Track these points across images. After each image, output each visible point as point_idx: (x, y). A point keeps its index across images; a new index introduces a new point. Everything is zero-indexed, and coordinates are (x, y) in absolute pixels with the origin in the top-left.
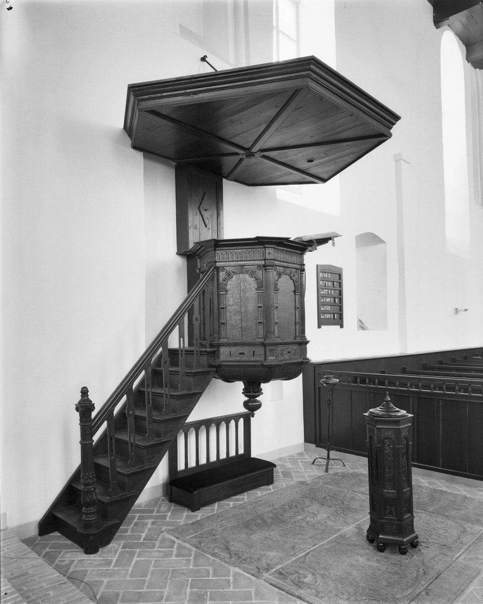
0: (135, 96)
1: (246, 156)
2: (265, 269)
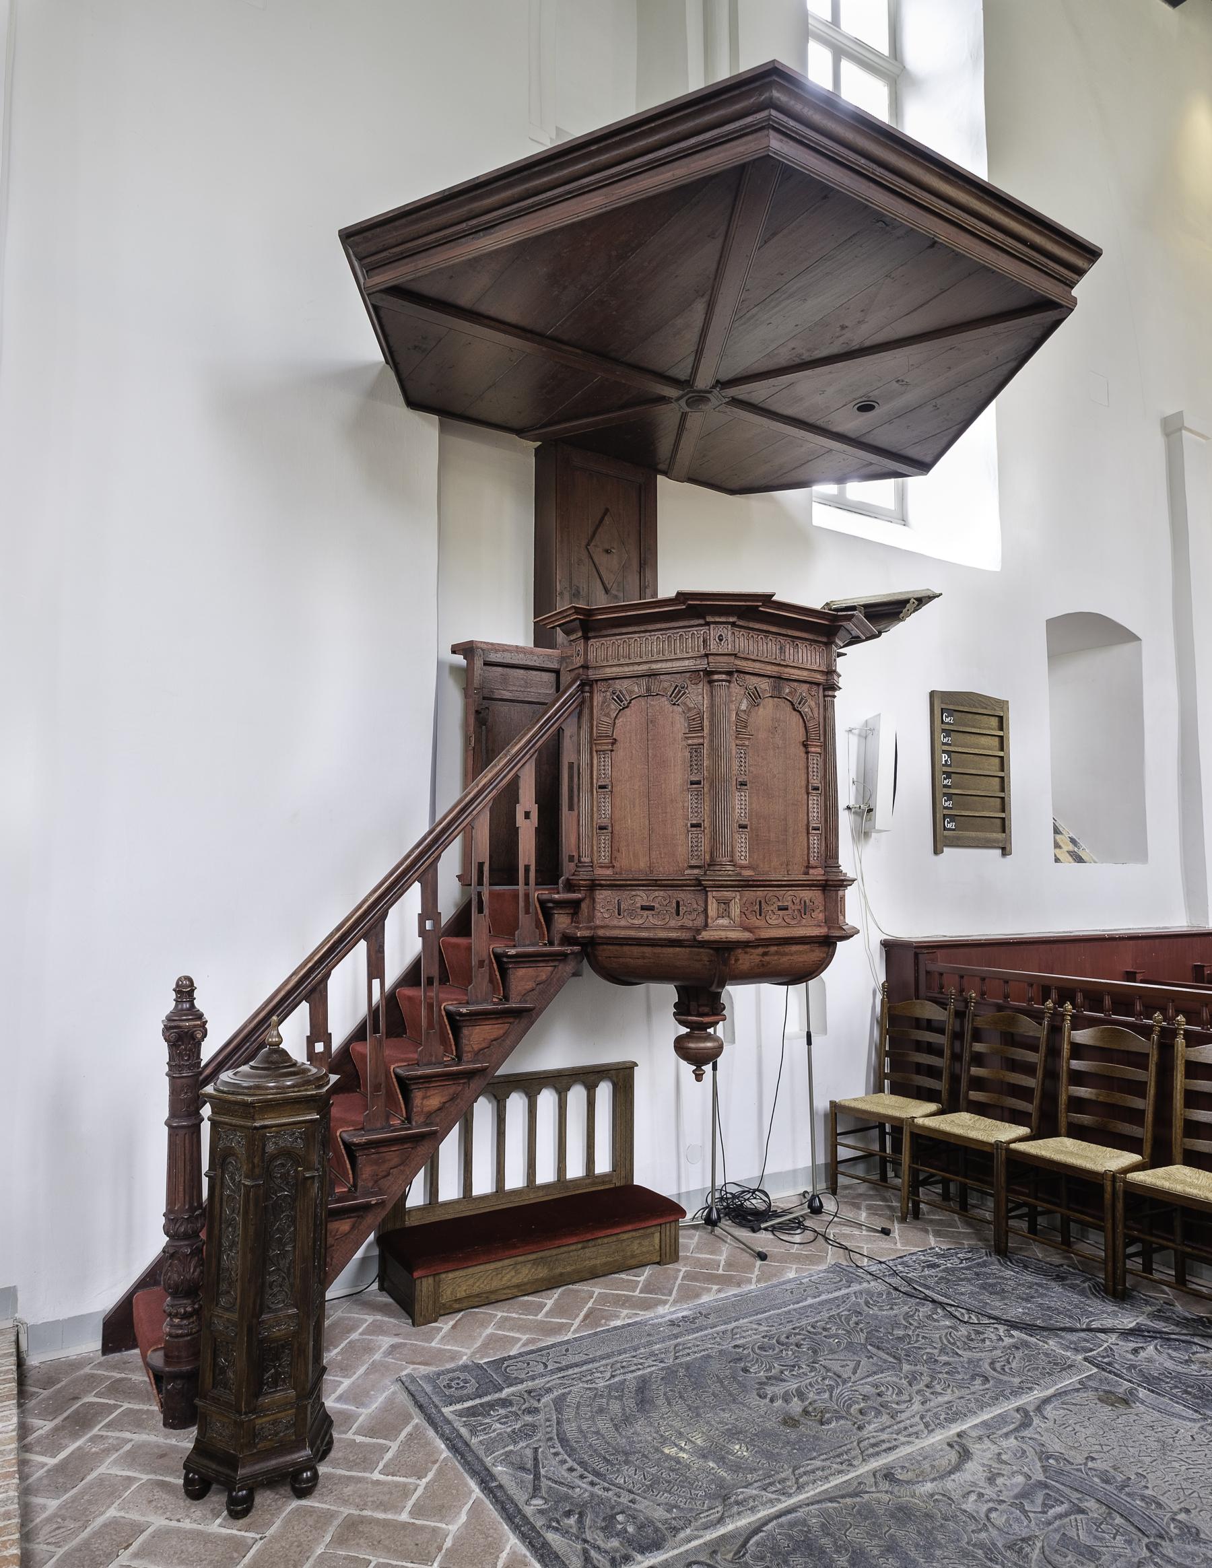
0: (360, 259)
1: (688, 404)
2: (711, 682)
